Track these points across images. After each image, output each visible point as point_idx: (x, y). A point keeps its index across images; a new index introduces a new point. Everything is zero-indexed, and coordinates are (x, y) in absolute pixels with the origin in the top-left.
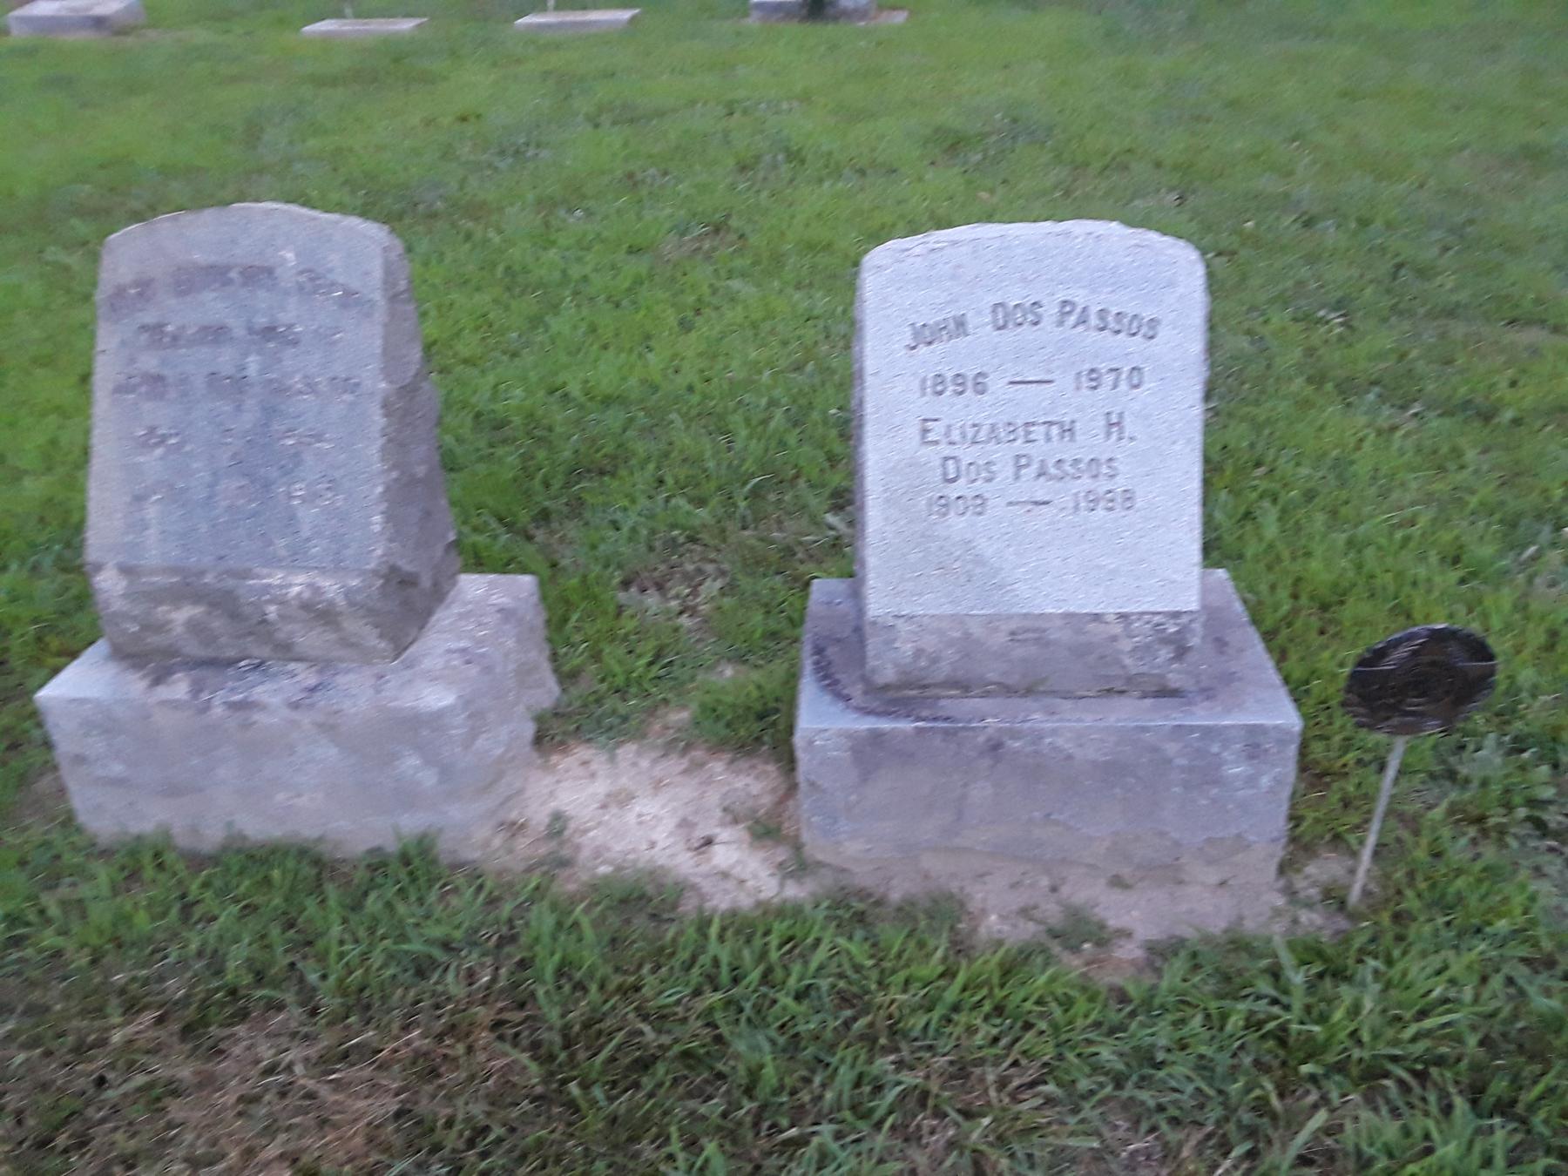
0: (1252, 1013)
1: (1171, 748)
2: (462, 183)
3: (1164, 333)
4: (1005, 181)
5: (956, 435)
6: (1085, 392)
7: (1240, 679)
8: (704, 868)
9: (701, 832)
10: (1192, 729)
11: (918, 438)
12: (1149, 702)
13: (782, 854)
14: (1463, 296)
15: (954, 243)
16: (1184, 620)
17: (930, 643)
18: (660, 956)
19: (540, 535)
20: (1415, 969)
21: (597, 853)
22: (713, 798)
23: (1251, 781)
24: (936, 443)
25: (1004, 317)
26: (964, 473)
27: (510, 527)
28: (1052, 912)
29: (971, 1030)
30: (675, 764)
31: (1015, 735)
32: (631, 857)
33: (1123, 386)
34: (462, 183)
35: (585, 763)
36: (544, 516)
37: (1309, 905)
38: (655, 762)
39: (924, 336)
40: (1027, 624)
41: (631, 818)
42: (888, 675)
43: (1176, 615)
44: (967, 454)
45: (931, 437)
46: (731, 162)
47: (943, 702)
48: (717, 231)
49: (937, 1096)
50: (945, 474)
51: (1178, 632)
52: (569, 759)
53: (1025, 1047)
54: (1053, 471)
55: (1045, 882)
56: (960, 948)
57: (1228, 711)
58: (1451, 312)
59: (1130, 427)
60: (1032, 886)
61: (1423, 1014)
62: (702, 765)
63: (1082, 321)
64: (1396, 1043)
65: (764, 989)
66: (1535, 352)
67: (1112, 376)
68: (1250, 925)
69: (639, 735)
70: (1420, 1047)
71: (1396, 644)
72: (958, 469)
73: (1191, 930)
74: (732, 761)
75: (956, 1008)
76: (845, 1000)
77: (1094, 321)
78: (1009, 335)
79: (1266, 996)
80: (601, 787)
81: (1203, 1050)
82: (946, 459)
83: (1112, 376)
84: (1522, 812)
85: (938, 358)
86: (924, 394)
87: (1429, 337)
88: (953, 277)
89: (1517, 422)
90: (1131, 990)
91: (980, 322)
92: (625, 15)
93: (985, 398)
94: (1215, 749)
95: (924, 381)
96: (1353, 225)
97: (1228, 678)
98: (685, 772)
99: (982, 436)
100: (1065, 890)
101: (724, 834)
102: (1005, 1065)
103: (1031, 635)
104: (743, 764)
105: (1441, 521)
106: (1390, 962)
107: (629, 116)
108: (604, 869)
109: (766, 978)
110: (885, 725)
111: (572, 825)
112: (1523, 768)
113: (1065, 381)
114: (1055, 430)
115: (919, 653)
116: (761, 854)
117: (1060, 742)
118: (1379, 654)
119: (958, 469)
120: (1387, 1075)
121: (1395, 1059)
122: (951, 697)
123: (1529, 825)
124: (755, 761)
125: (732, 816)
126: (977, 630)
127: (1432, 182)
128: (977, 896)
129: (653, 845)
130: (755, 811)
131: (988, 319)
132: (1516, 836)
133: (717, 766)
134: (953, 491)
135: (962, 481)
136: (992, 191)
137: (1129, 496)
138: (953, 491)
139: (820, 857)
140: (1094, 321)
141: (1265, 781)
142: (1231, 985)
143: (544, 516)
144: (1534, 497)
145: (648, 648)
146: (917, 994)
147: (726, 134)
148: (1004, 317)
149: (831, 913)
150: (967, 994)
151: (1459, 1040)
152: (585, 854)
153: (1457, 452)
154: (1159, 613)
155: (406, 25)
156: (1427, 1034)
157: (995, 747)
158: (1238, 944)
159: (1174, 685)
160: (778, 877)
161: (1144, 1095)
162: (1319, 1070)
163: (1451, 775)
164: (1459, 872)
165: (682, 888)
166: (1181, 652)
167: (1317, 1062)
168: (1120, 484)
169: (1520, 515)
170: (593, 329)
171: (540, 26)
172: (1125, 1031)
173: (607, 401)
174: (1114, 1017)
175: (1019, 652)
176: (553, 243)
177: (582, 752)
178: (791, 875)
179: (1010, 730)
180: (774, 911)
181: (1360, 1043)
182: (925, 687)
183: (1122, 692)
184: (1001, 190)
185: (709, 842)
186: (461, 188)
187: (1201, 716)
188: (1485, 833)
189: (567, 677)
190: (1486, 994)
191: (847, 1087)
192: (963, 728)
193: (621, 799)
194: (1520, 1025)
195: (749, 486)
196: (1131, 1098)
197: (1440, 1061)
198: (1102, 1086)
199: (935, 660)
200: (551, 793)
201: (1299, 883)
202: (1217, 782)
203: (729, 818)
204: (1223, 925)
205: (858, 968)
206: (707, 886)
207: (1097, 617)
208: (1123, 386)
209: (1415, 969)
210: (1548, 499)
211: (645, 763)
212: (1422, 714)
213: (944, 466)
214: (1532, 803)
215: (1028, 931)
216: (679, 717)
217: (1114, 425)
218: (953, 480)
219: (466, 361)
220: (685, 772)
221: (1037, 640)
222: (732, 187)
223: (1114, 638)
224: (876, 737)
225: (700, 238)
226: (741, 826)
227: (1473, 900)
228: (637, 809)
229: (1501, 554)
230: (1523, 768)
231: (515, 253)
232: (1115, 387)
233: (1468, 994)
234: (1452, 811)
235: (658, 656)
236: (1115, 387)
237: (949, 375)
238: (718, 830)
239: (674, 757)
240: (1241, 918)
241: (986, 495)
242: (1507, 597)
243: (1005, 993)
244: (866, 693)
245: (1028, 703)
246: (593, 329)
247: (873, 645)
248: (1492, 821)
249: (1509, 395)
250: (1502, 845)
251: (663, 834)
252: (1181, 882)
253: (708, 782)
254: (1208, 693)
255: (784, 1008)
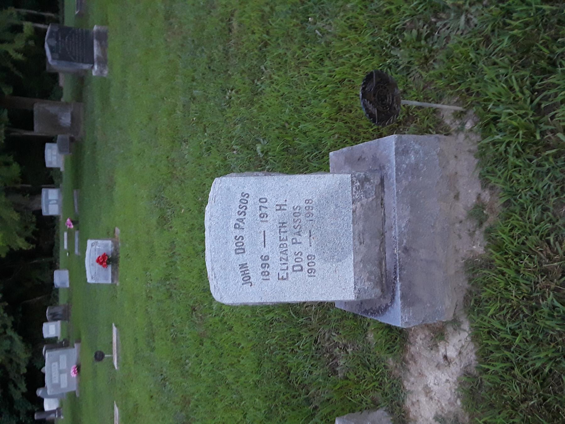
0: (514, 155)
1: (404, 183)
2: (176, 403)
3: (246, 191)
4: (178, 203)
5: (284, 267)
6: (268, 219)
7: (375, 154)
8: (457, 360)
9: (442, 361)
10: (397, 175)
11: (285, 281)
12: (385, 190)
13: (450, 329)
14: (221, 47)
15: (213, 269)
16: (354, 179)
17: (365, 276)
18: (499, 389)
19: (316, 404)
20: (491, 90)
21: (451, 404)
22: (426, 353)
23: (417, 153)
24: (287, 274)
25: (240, 250)
26: (299, 263)
27: (313, 415)
28: (471, 224)
29: (527, 267)
30: (412, 367)
31: (401, 243)
32: (453, 391)
33: (266, 205)
34: (176, 403)
35: (413, 404)
36: (308, 401)
37: (463, 124)
38: (411, 374)
39: (247, 279)
40: (357, 237)
41: (435, 388)
42: (378, 291)
43: (353, 182)
44: (291, 263)
45: (285, 277)
46: (168, 301)
47: (388, 268)
48: (194, 310)
49: (556, 284)
50: (299, 271)
51: (359, 181)
52: (411, 410)
53: (534, 246)
54: (298, 230)
55: (457, 225)
56: (489, 264)
57: (389, 161)
58: (226, 52)
59: (282, 202)
60: (460, 230)
61: (511, 88)
62: (412, 356)
63: (242, 220)
64: (525, 101)
65: (512, 349)
66: (240, 24)
67: (263, 209)
68: (474, 148)
69: (400, 380)
70: (527, 92)
71: (367, 109)
72: (297, 266)
73: (476, 171)
74: (410, 343)
75: (518, 272)
76: (515, 316)
77: (242, 216)
78: (247, 248)
79: (506, 147)
80: (423, 399)
81: (531, 175)
82: (294, 271)
83: (263, 209)
84: (423, 42)
85: (255, 274)
86: (269, 279)
87: (236, 61)
88: (225, 269)
89: (268, 33)
90: (505, 199)
91: (242, 259)
92: (115, 329)
93: (270, 256)
94: (404, 166)
95: (264, 279)
96: (195, 84)
97: (375, 159)
98: (415, 362)
99: (285, 257)
100: (461, 217)
101: (442, 351)
102: (542, 255)
103: (361, 237)
104: (411, 339)
105: (306, 64)
106: (490, 100)
107: (151, 336)
108: (459, 402)
109: (508, 348)
110: (399, 293)
111: (440, 413)
112: (404, 41)
113: (264, 226)
114: (283, 230)
115: (369, 279)
116: (450, 338)
117: (404, 225)
118: (371, 116)
119: (297, 266)
120: (539, 104)
121: (532, 101)
122: (386, 265)
123: (428, 40)
124: (410, 335)
125: (434, 347)
126: (359, 258)
127: (179, 53)
128: (464, 251)
129: (447, 381)
130: (432, 338)
131: (241, 255)
132: (433, 45)
133: (412, 349)
134: (306, 267)
135: (302, 263)
136: (181, 208)
137: (307, 201)
138: (306, 267)
139: (451, 315)
140: (242, 216)
141: (417, 147)
142: (501, 160)
143: (308, 401)
144: (297, 29)
145: (362, 371)
146: (512, 288)
147: (158, 301)
148: (240, 250)
149: (476, 314)
150: (511, 267)
151: (523, 77)
152: (452, 409)
153: (279, 56)
154: (352, 189)
155: (116, 410)
156: (521, 88)
157: (406, 250)
158: (481, 154)
159: (379, 181)
160: (461, 332)
161: (552, 200)
162: (538, 131)
163: (408, 68)
164: (449, 68)
165: (466, 373)
166: (367, 179)
167: (535, 132)
168: (303, 204)
169: (303, 35)
170: (232, 365)
171: (118, 361)
172: (523, 204)
173: (260, 365)
174: (518, 209)
175: (367, 241)
176: (199, 373)
177: (408, 403)
178: (459, 326)
179: (399, 244)
180: (475, 337)
181: (526, 114)
182: (382, 275)
183: (382, 200)
184: (181, 204)
185: (445, 357)
186: (178, 404)
187: (392, 172)
188: (432, 57)
189: (376, 405)
190: (501, 64)
191: (554, 322)
192: (399, 262)
193: (427, 391)
194: (515, 51)
195: (294, 315)
196: (554, 206)
197: (533, 84)
198: (548, 216)
199: (371, 273)
200: (427, 420)
201: (454, 127)
202: (417, 164)
203: (434, 348)
204: (473, 158)
205: (501, 309)
206: (465, 361)
207: (354, 212)
208: (266, 205)
209: (491, 90)
210: (298, 25)
211: (412, 379)
212: (393, 96)
213: (296, 271)
214: (419, 38)
215: (479, 234)
216: (391, 363)
217: (280, 207)
218: (302, 267)
219: (245, 417)
220: (415, 362)
221: (363, 234)
222: (178, 302)
223: (362, 205)
224: (403, 297)
225: (197, 317)
226: (439, 344)
227: (461, 65)
228: (431, 384)
229: (319, 44)
230: (404, 41)
231: (202, 389)
232: (266, 208)
233: (502, 71)
234: (423, 68)
235: (364, 365)
236: (266, 208)
237: (262, 270)
238: (440, 353)
239: (409, 367)
240: (470, 151)
241: (308, 254)
242: (336, 44)
243: (511, 253)
244: (385, 298)
245: (387, 235)
246: (232, 365)
247: (365, 297)
248: (427, 54)
249: (256, 36)
250: (437, 51)
251: (443, 377)
252: (456, 173)
253: (420, 355)
254: (382, 168)
255: (520, 341)
